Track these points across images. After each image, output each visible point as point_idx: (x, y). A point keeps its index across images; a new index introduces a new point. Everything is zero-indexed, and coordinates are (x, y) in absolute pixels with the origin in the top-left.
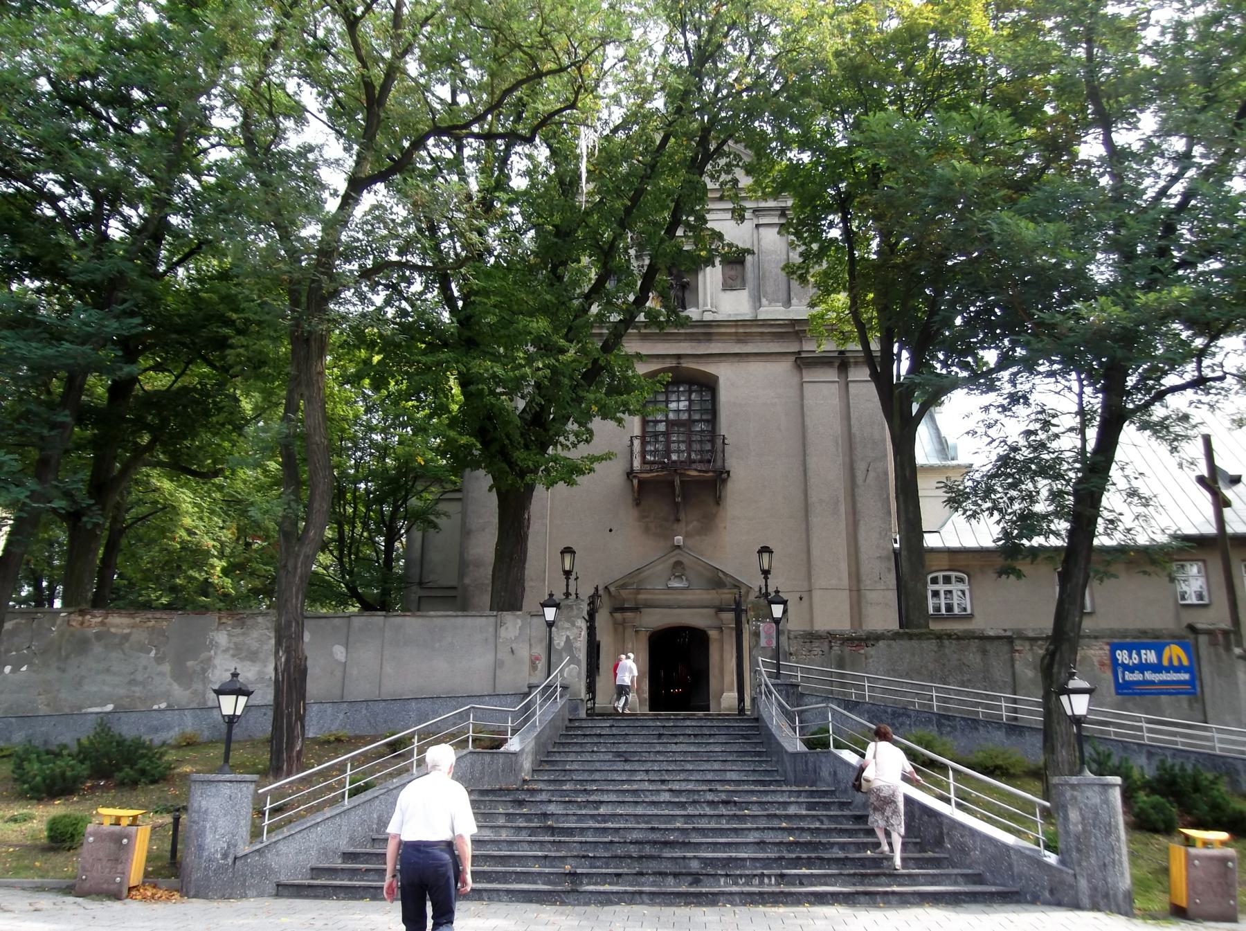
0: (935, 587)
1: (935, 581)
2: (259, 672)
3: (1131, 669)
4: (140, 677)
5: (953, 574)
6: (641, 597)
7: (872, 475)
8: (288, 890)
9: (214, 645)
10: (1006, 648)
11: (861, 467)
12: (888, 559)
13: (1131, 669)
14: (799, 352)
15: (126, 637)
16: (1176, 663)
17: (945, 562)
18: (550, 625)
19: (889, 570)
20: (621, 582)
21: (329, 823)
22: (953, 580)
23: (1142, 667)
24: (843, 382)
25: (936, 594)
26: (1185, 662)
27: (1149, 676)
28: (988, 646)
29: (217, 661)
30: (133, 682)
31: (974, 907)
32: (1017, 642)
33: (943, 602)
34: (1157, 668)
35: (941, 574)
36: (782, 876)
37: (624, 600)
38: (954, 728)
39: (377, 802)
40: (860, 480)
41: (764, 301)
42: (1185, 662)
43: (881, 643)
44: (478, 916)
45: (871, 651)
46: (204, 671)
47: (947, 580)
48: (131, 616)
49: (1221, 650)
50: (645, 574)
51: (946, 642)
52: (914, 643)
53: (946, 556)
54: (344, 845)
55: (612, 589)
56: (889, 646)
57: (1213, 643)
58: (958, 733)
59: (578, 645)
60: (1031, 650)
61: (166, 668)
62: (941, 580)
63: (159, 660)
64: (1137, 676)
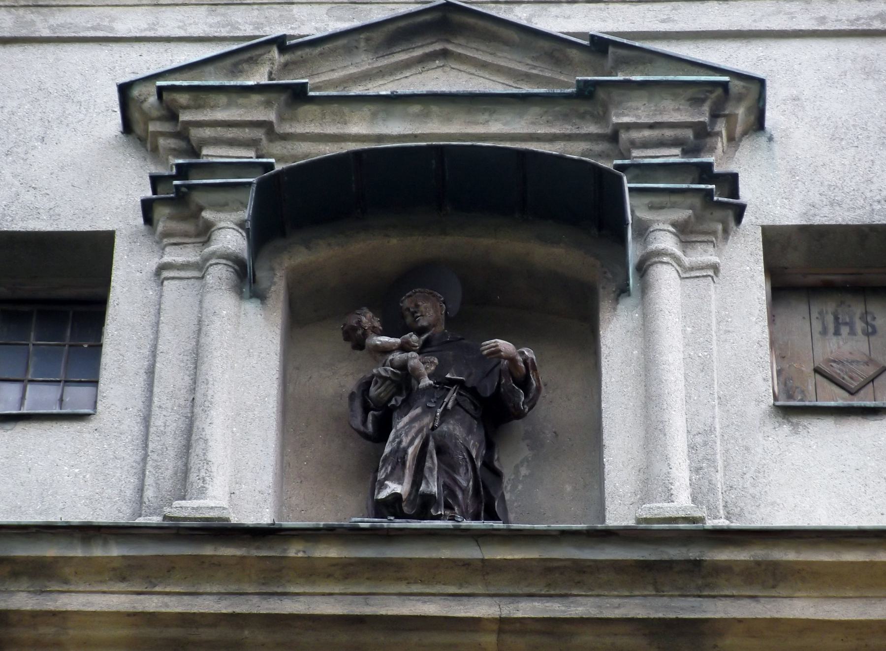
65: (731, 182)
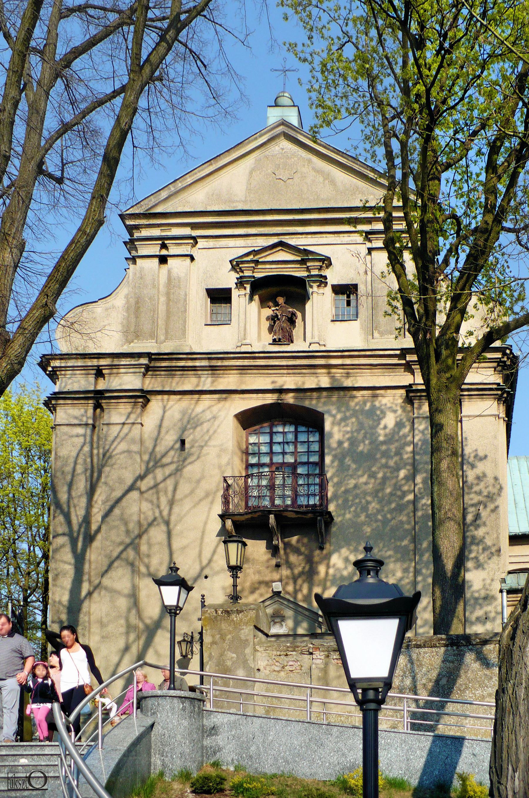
14: (410, 385)
41: (376, 334)
65: (325, 277)
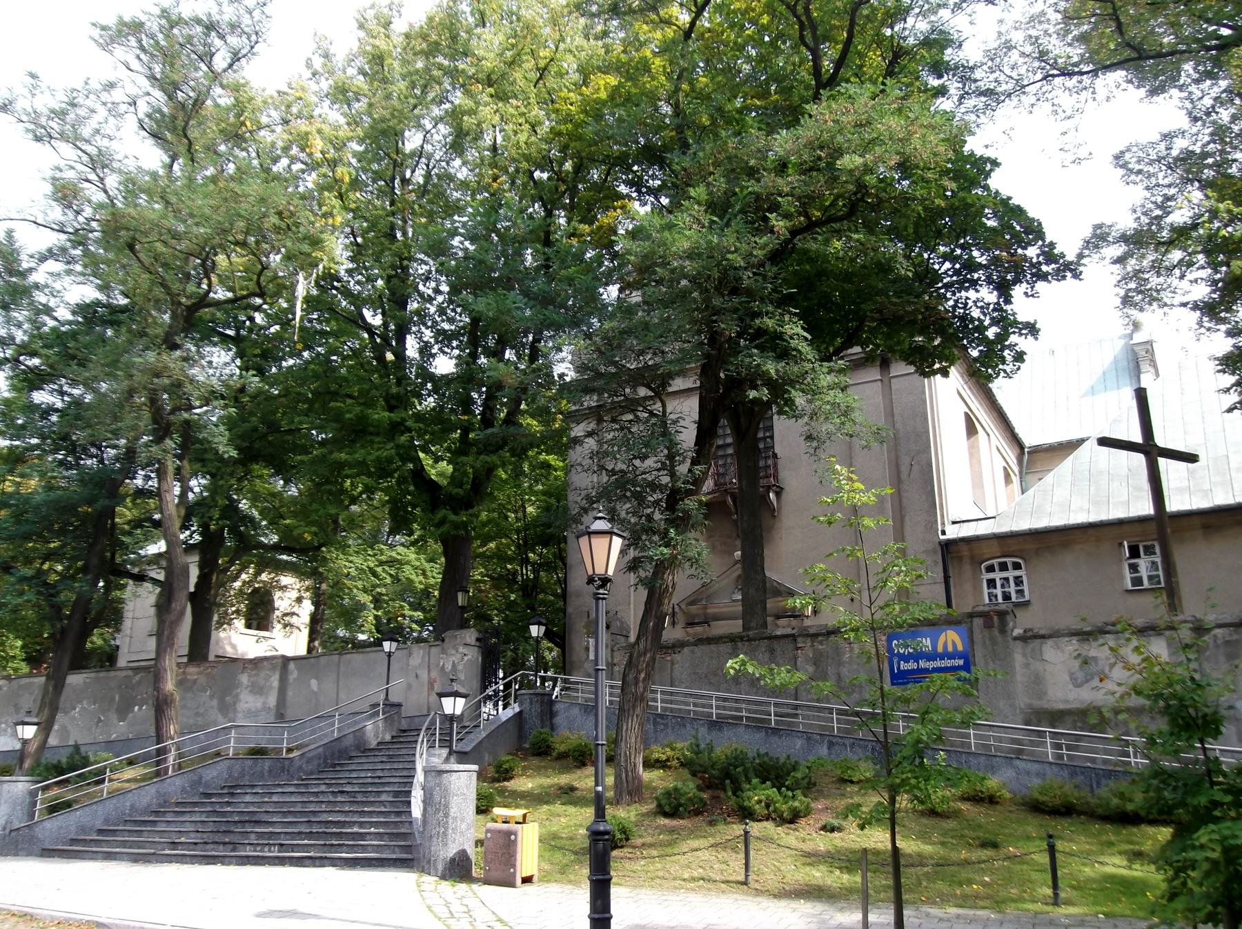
0: (991, 576)
1: (991, 569)
2: (264, 703)
3: (906, 658)
4: (201, 711)
5: (1009, 560)
6: (709, 611)
7: (916, 468)
8: (48, 853)
9: (240, 684)
10: (791, 646)
11: (905, 461)
12: (935, 551)
13: (906, 658)
15: (195, 681)
16: (950, 649)
17: (995, 548)
18: (389, 655)
19: (936, 563)
20: (690, 600)
21: (86, 809)
22: (1010, 566)
23: (916, 657)
24: (886, 380)
25: (992, 583)
26: (960, 648)
27: (923, 664)
28: (775, 644)
29: (242, 696)
30: (197, 714)
31: (56, 859)
32: (799, 639)
33: (998, 591)
34: (932, 657)
35: (995, 562)
36: (282, 845)
37: (694, 616)
38: (666, 725)
39: (130, 795)
40: (904, 476)
42: (960, 648)
43: (686, 650)
44: (842, 910)
45: (677, 657)
46: (235, 703)
47: (1003, 567)
48: (198, 666)
49: (996, 632)
50: (712, 590)
51: (740, 644)
52: (713, 647)
53: (995, 542)
54: (99, 824)
55: (683, 606)
56: (693, 652)
57: (988, 625)
58: (669, 731)
59: (460, 667)
60: (812, 646)
61: (215, 702)
62: (997, 568)
63: (212, 697)
64: (911, 665)
